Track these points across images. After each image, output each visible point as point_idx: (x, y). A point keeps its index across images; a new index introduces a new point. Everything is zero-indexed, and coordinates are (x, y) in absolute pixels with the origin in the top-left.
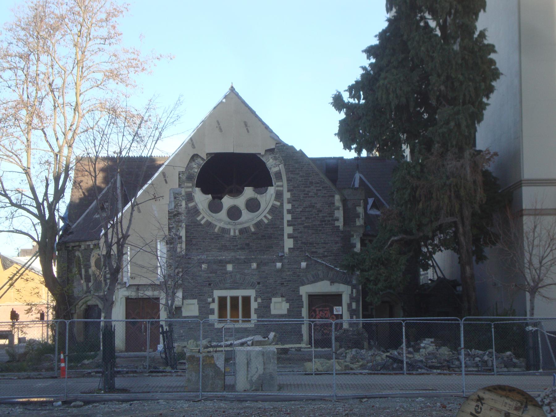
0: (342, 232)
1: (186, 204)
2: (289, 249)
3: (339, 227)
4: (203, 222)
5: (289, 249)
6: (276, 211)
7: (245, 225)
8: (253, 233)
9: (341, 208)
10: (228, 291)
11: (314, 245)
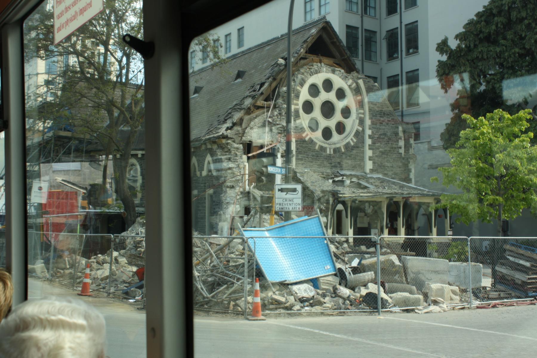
3: (401, 154)
4: (307, 139)
6: (359, 135)
7: (338, 146)
9: (403, 138)
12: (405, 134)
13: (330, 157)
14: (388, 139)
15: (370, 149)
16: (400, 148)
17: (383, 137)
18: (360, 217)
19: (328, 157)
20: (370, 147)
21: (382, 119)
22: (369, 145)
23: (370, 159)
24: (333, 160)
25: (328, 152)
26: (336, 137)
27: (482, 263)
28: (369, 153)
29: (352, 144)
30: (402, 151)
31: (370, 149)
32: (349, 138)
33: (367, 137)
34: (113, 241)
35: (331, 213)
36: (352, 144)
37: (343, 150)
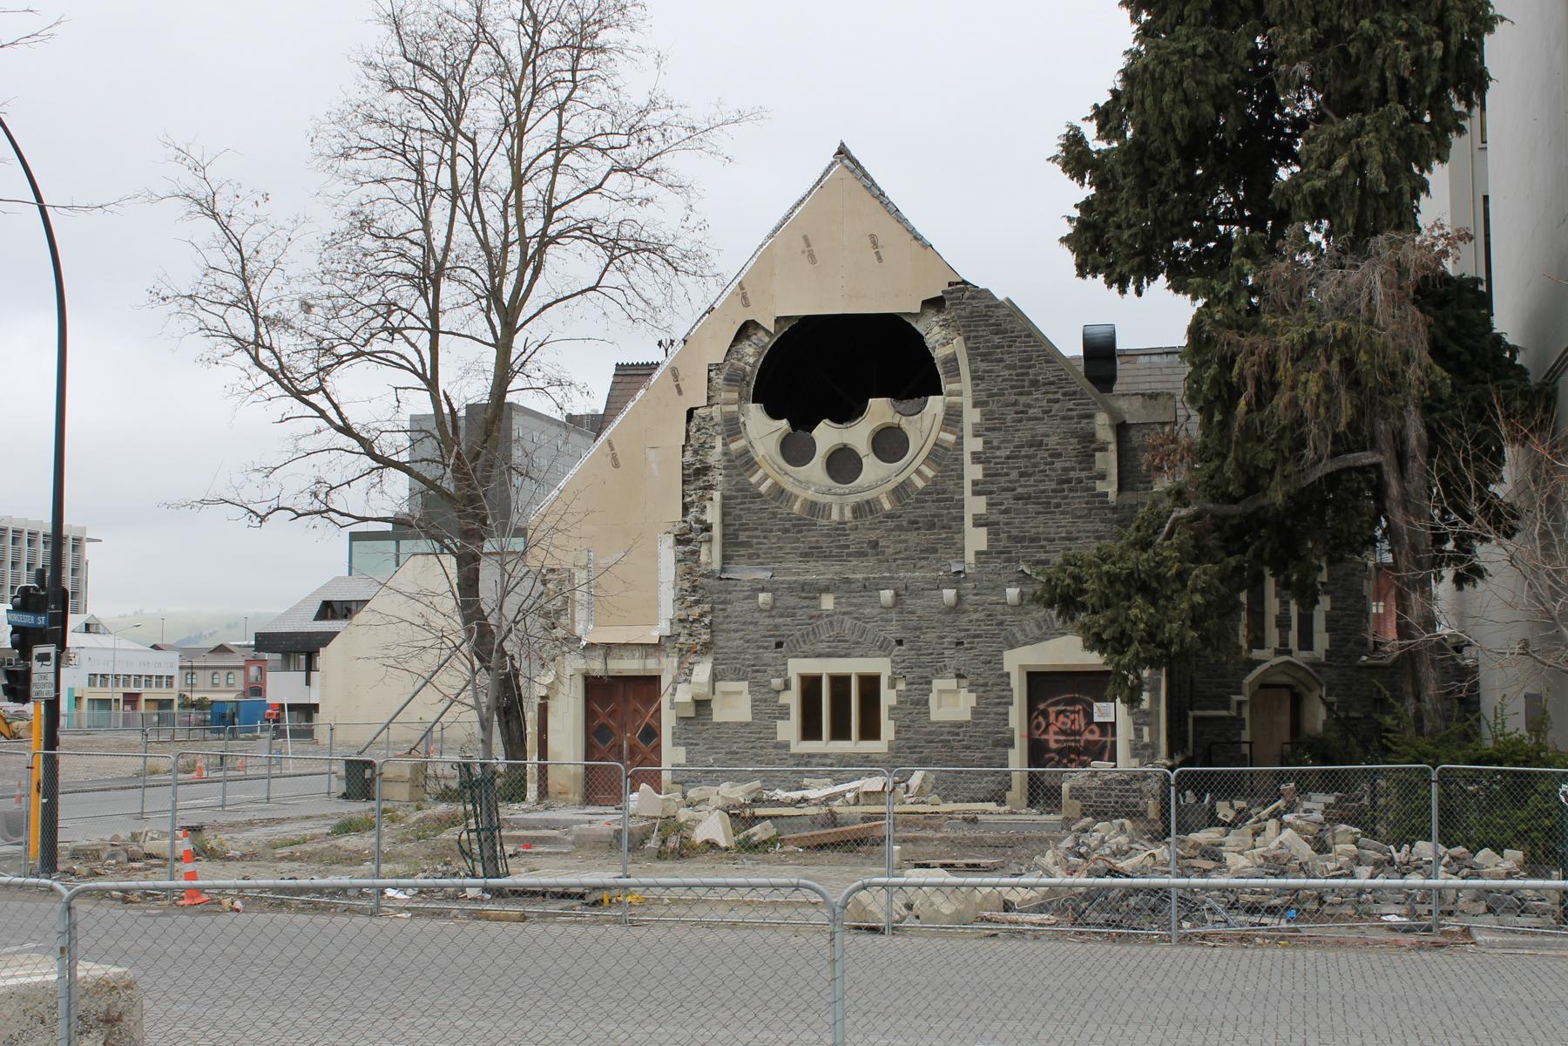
0: (1114, 509)
1: (725, 445)
2: (978, 553)
3: (1106, 494)
4: (763, 489)
5: (978, 553)
6: (944, 458)
8: (889, 516)
10: (823, 660)
11: (1043, 543)
12: (52, 696)
13: (844, 530)
14: (1051, 456)
15: (975, 493)
16: (1103, 476)
17: (1032, 451)
18: (941, 692)
19: (837, 529)
20: (978, 488)
21: (1023, 399)
22: (975, 483)
23: (979, 522)
24: (851, 537)
25: (835, 516)
26: (873, 469)
27: (1130, 819)
28: (975, 505)
29: (920, 484)
30: (1110, 488)
31: (975, 493)
32: (914, 468)
33: (967, 458)
34: (1089, 715)
35: (500, 720)
36: (920, 484)
37: (887, 506)
